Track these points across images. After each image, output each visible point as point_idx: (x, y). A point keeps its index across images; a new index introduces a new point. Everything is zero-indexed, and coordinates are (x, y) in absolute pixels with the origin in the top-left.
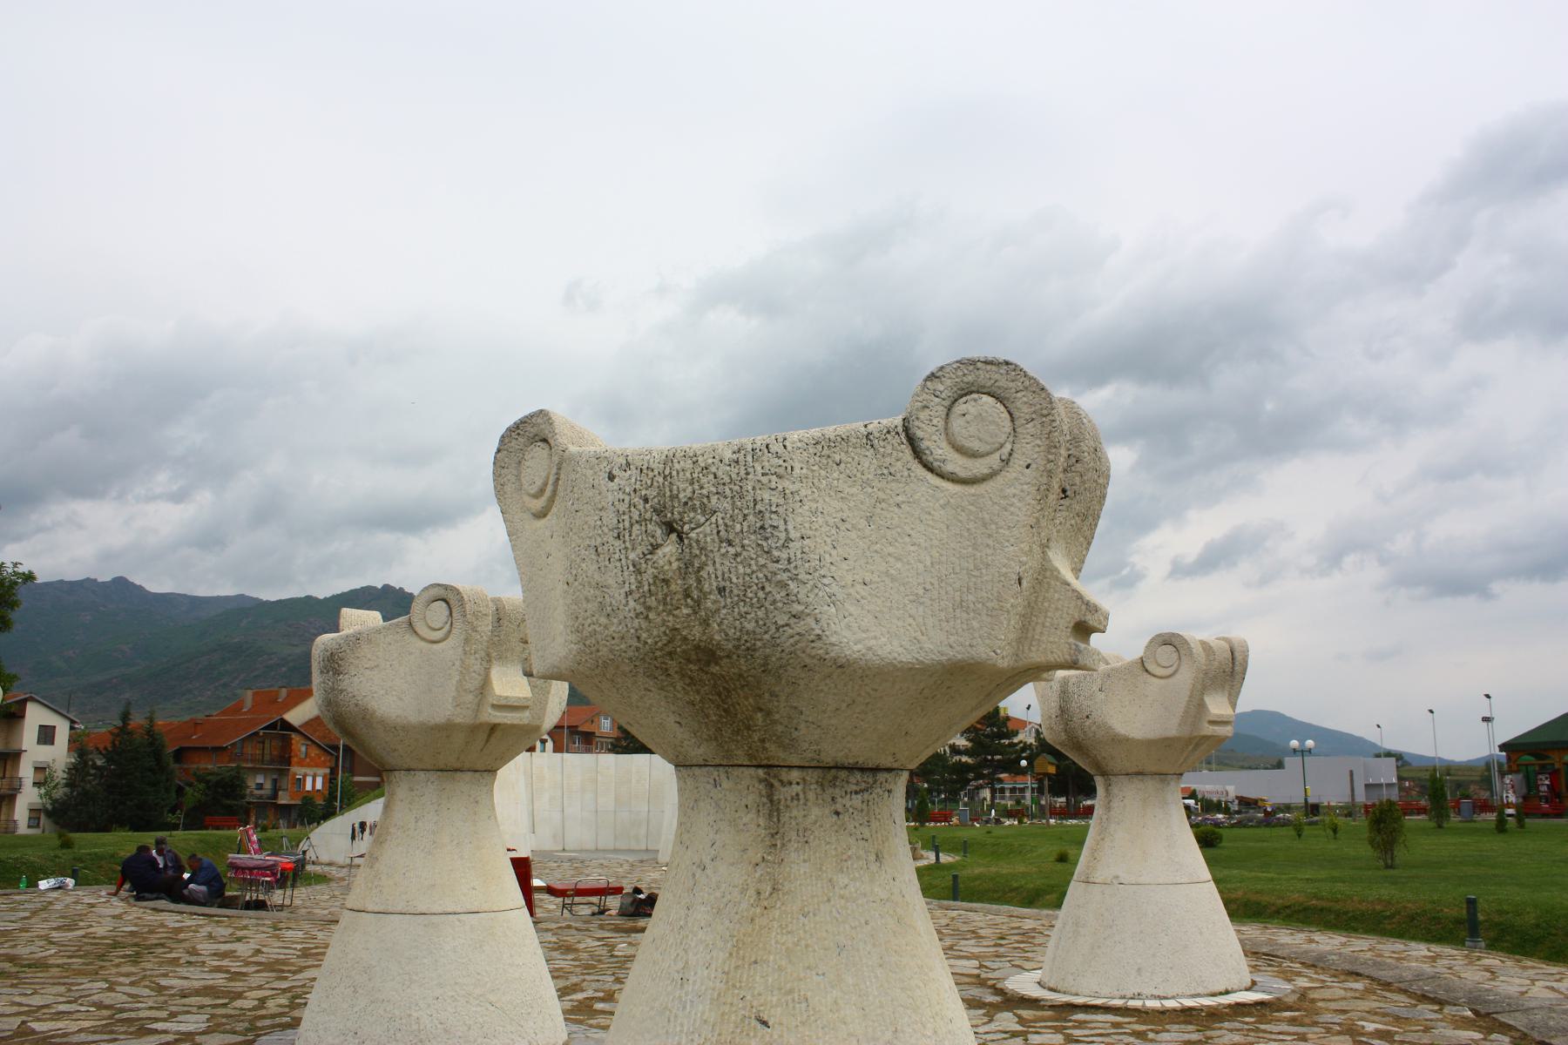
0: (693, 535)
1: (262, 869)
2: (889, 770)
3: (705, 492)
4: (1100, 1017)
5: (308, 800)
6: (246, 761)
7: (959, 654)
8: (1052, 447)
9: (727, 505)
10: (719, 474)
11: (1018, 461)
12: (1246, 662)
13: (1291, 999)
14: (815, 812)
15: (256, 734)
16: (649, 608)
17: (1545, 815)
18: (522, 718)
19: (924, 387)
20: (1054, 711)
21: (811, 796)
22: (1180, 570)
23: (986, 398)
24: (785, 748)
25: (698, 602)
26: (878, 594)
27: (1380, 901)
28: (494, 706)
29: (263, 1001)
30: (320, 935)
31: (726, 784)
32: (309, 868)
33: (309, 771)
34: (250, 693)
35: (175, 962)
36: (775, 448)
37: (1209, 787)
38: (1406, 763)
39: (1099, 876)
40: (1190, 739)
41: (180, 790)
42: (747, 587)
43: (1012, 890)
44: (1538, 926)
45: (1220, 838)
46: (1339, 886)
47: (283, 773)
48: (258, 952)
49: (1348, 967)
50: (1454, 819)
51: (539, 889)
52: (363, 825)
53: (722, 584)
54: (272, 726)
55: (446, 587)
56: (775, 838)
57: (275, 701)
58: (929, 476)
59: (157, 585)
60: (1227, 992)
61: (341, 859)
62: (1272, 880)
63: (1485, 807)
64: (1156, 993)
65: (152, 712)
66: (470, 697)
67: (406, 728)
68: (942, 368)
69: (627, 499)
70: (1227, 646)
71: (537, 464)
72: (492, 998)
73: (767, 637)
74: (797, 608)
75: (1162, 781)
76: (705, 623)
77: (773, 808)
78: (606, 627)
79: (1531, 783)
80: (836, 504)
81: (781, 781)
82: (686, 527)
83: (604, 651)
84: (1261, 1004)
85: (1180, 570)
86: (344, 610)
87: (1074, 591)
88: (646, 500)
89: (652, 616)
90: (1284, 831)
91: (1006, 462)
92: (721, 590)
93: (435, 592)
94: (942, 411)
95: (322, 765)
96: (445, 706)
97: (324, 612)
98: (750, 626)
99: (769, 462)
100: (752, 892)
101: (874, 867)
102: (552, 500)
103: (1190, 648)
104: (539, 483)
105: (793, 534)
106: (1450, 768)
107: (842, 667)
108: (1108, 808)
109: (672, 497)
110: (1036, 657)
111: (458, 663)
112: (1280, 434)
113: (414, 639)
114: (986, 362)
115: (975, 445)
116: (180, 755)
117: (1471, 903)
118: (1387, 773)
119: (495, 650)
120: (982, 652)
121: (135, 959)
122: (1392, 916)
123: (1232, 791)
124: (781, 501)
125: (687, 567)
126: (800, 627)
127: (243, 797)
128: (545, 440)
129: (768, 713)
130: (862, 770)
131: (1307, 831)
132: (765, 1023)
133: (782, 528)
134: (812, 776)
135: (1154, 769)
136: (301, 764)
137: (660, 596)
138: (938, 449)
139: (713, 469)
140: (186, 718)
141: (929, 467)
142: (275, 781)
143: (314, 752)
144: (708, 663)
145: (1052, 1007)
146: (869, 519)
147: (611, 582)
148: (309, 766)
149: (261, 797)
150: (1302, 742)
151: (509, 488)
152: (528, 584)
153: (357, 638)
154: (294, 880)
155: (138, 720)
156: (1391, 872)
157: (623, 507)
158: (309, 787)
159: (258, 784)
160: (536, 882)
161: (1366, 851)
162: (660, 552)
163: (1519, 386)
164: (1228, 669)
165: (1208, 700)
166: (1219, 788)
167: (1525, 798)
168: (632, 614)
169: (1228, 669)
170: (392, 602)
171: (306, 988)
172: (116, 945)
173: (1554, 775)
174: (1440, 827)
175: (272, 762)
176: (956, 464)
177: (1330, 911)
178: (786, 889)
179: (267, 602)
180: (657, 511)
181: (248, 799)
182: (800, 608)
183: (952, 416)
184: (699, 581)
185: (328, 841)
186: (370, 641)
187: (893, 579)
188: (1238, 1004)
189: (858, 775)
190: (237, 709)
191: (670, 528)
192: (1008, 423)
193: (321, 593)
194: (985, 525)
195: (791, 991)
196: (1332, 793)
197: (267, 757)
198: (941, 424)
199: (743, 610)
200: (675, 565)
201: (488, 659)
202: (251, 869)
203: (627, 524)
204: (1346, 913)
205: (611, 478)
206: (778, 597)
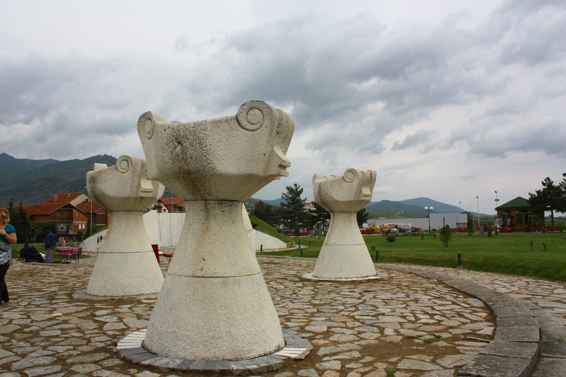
1: (68, 251)
4: (327, 283)
5: (80, 233)
6: (57, 219)
8: (272, 122)
11: (264, 126)
14: (217, 211)
15: (60, 209)
17: (509, 232)
18: (151, 195)
20: (317, 193)
21: (216, 207)
22: (397, 147)
26: (228, 159)
27: (438, 256)
29: (74, 284)
30: (90, 269)
31: (196, 205)
32: (83, 254)
33: (80, 222)
34: (57, 195)
35: (44, 276)
36: (204, 123)
37: (402, 224)
40: (357, 201)
41: (33, 230)
42: (197, 157)
44: (482, 262)
47: (71, 223)
48: (70, 273)
49: (410, 271)
51: (161, 255)
52: (101, 237)
54: (66, 207)
55: (127, 156)
56: (207, 217)
57: (66, 198)
58: (242, 129)
59: (18, 156)
60: (367, 277)
61: (94, 250)
65: (21, 202)
67: (116, 199)
72: (144, 276)
74: (209, 161)
76: (188, 165)
77: (207, 210)
79: (504, 221)
80: (219, 137)
83: (165, 173)
85: (397, 147)
86: (95, 164)
90: (418, 237)
91: (261, 126)
92: (191, 157)
94: (245, 113)
95: (85, 220)
96: (127, 191)
97: (90, 163)
98: (198, 166)
100: (202, 230)
101: (232, 224)
102: (152, 135)
104: (149, 130)
105: (208, 144)
108: (334, 223)
112: (436, 97)
113: (117, 172)
115: (254, 122)
116: (32, 217)
117: (459, 255)
120: (255, 172)
121: (32, 276)
122: (440, 261)
123: (410, 225)
125: (183, 152)
126: (210, 166)
127: (56, 232)
129: (204, 187)
130: (229, 201)
134: (216, 202)
136: (77, 220)
138: (244, 123)
140: (33, 204)
142: (67, 226)
143: (81, 215)
145: (314, 281)
146: (227, 140)
148: (80, 220)
149: (63, 232)
150: (429, 207)
151: (141, 131)
152: (147, 156)
153: (100, 172)
154: (78, 257)
155: (16, 205)
157: (168, 138)
158: (80, 228)
159: (61, 227)
160: (160, 253)
163: (523, 81)
164: (370, 180)
165: (363, 189)
166: (405, 224)
167: (502, 226)
169: (370, 180)
170: (110, 161)
171: (87, 281)
172: (24, 273)
173: (512, 218)
174: (470, 235)
175: (66, 219)
176: (249, 126)
179: (61, 162)
180: (176, 139)
181: (58, 233)
185: (90, 244)
186: (104, 173)
187: (233, 154)
189: (228, 202)
190: (53, 200)
192: (262, 117)
193: (82, 157)
197: (64, 218)
198: (245, 117)
201: (140, 177)
202: (64, 251)
205: (165, 130)
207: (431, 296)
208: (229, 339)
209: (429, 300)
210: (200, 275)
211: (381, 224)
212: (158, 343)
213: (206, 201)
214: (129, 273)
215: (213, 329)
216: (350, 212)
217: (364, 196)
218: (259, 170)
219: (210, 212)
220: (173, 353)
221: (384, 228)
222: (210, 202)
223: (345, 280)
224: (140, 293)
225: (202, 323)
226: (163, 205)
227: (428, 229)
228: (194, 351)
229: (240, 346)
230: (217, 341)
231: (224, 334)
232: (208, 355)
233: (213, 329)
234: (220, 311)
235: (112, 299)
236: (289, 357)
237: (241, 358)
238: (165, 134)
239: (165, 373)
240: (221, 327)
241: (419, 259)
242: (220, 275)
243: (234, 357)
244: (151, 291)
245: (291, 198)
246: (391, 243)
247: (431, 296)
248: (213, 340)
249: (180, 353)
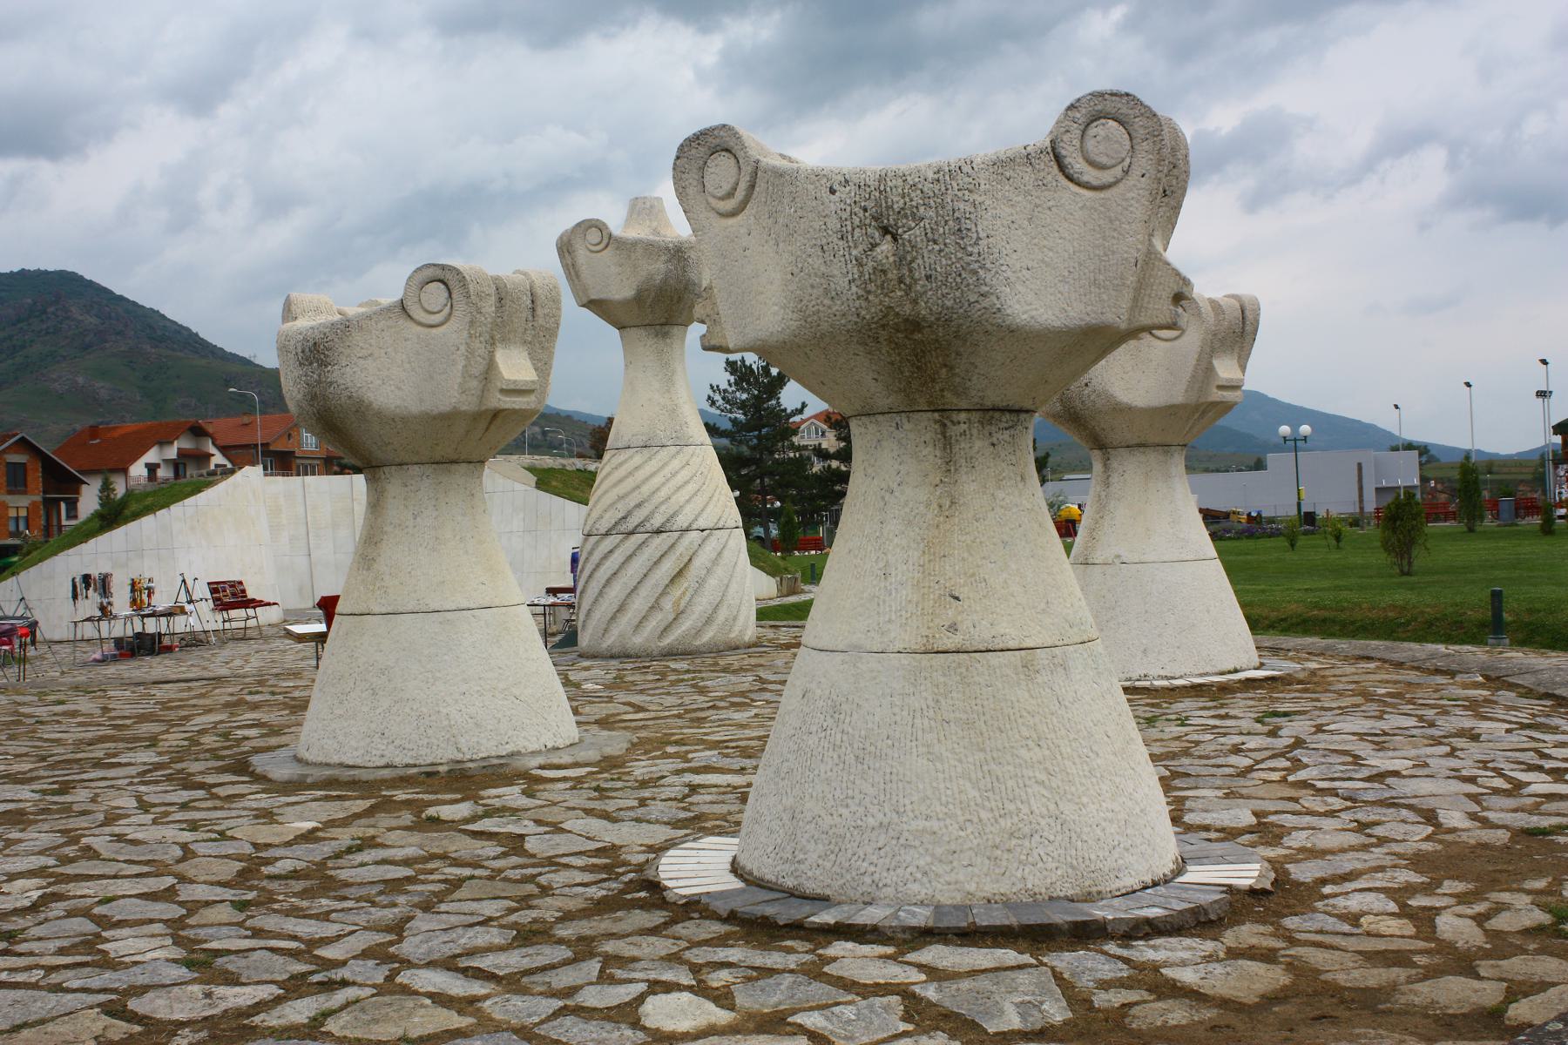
0: (906, 236)
2: (1027, 411)
7: (1092, 319)
9: (932, 213)
11: (1136, 172)
12: (1257, 322)
13: (1301, 676)
14: (978, 444)
16: (869, 292)
19: (1066, 115)
21: (975, 432)
23: (1111, 123)
24: (957, 395)
25: (910, 287)
27: (1393, 607)
28: (502, 391)
31: (907, 426)
36: (966, 169)
38: (1432, 459)
39: (1098, 557)
40: (1197, 407)
42: (948, 274)
46: (1345, 594)
50: (1488, 523)
55: (443, 267)
56: (949, 464)
58: (1071, 185)
60: (1236, 671)
62: (1263, 591)
63: (1530, 508)
64: (1163, 673)
66: (474, 383)
70: (1238, 305)
71: (721, 172)
72: (516, 691)
75: (1166, 452)
76: (915, 302)
77: (946, 442)
80: (1008, 210)
84: (1267, 679)
88: (865, 210)
91: (1126, 172)
92: (928, 277)
93: (429, 273)
96: (450, 391)
98: (949, 303)
99: (963, 180)
100: (935, 506)
101: (1021, 485)
103: (1198, 308)
105: (982, 235)
106: (1493, 464)
107: (1015, 334)
109: (888, 208)
110: (1145, 320)
111: (463, 348)
113: (409, 324)
114: (1112, 94)
115: (1104, 160)
118: (1406, 474)
119: (499, 333)
120: (1110, 317)
122: (1408, 623)
125: (901, 260)
126: (985, 303)
128: (727, 150)
129: (952, 368)
131: (1302, 541)
132: (957, 599)
134: (975, 416)
135: (1157, 440)
138: (1077, 165)
141: (1070, 178)
144: (912, 332)
147: (836, 272)
150: (1295, 428)
151: (691, 191)
156: (1405, 579)
161: (1380, 558)
162: (878, 250)
165: (1216, 363)
174: (1471, 530)
176: (1090, 175)
177: (1334, 621)
183: (1087, 138)
187: (1047, 265)
188: (1248, 680)
191: (885, 231)
192: (1128, 143)
195: (973, 575)
196: (1333, 496)
198: (1076, 142)
200: (891, 259)
201: (492, 342)
204: (1353, 623)
205: (833, 192)
207: (1510, 722)
208: (1059, 838)
209: (1508, 731)
210: (950, 645)
212: (828, 865)
213: (944, 413)
214: (465, 681)
215: (1012, 807)
216: (1165, 447)
217: (1221, 387)
218: (1116, 313)
219: (956, 449)
220: (889, 891)
222: (955, 417)
223: (1165, 683)
224: (510, 748)
225: (973, 793)
226: (212, 450)
227: (1294, 512)
228: (961, 877)
229: (1093, 857)
230: (1027, 843)
231: (1043, 823)
232: (1004, 887)
233: (1012, 807)
234: (1023, 752)
235: (429, 774)
236: (1230, 886)
237: (1099, 893)
238: (832, 204)
239: (905, 941)
240: (1032, 801)
241: (1324, 621)
242: (1012, 644)
243: (1078, 890)
244: (542, 740)
245: (743, 405)
247: (1510, 722)
248: (1014, 842)
249: (915, 887)
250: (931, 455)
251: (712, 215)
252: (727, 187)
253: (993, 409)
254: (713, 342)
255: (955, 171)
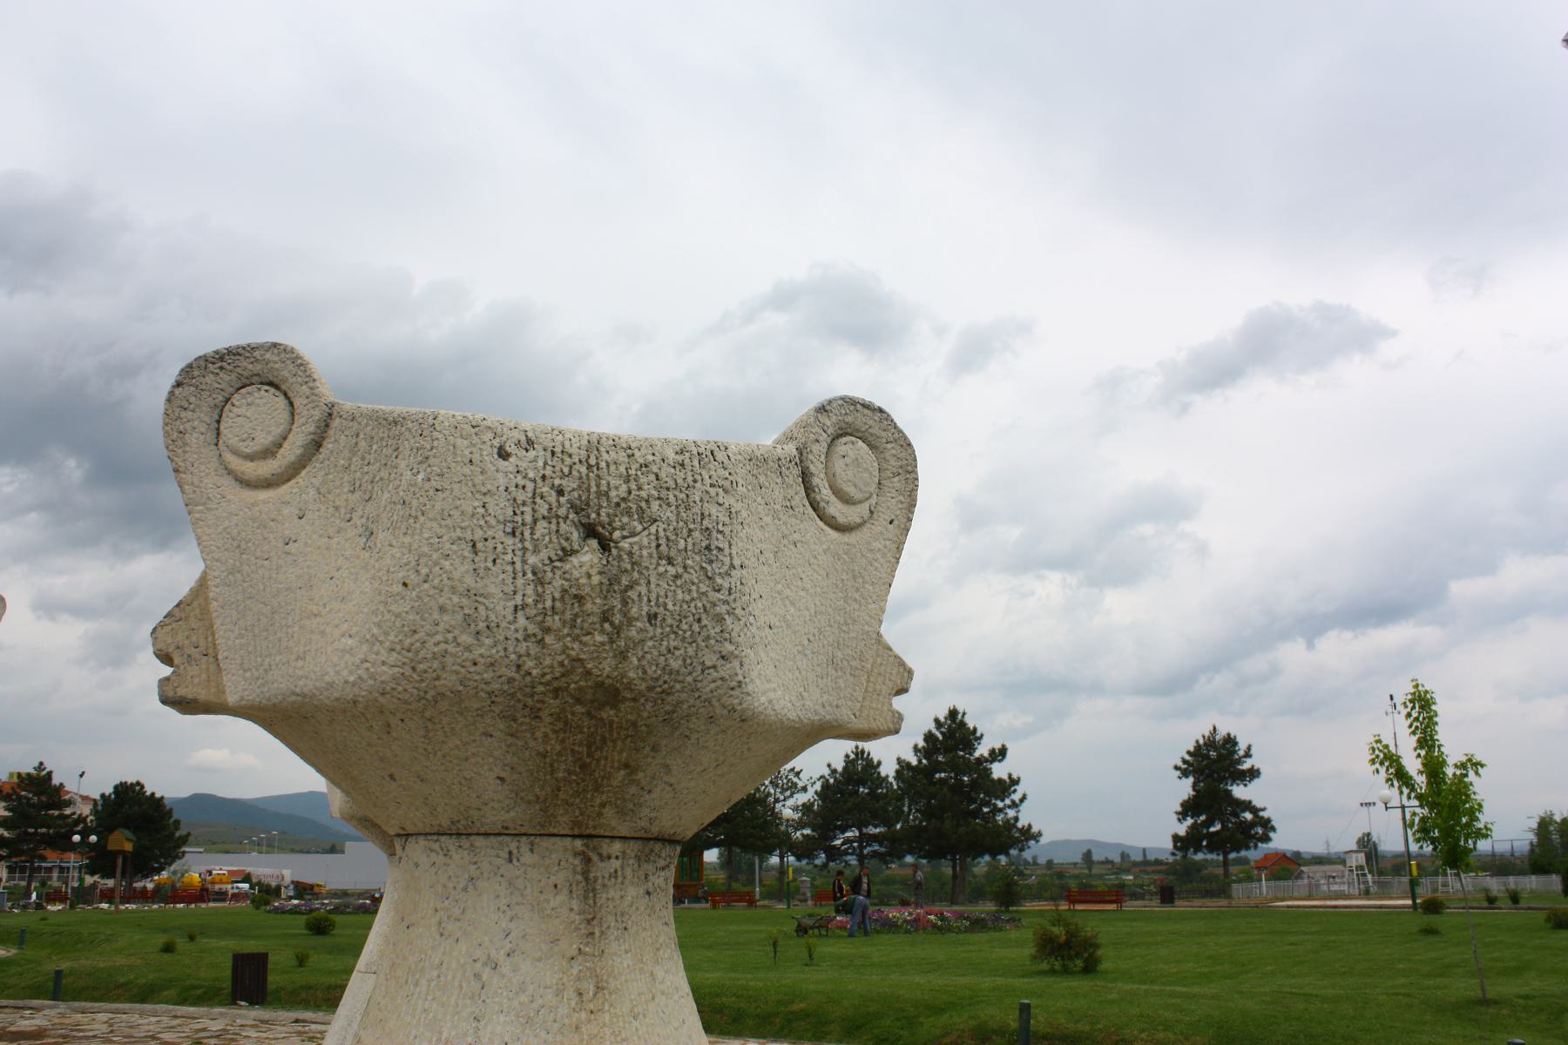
0: (625, 545)
3: (643, 494)
9: (669, 514)
10: (663, 475)
14: (632, 892)
16: (547, 630)
21: (628, 872)
24: (621, 812)
25: (618, 630)
31: (527, 858)
36: (720, 456)
43: (121, 986)
45: (332, 925)
53: (654, 609)
56: (591, 924)
68: (830, 402)
69: (530, 486)
71: (256, 417)
73: (689, 679)
76: (622, 655)
77: (589, 887)
78: (468, 649)
81: (600, 855)
82: (617, 534)
87: (896, 657)
88: (560, 492)
89: (549, 639)
92: (652, 617)
98: (675, 664)
100: (570, 993)
105: (737, 562)
109: (599, 494)
115: (851, 490)
123: (288, 875)
124: (727, 520)
133: (727, 551)
134: (633, 848)
137: (568, 616)
139: (655, 469)
144: (601, 706)
147: (492, 589)
151: (193, 439)
162: (575, 560)
166: (276, 872)
168: (520, 636)
176: (835, 508)
178: (612, 986)
182: (731, 648)
184: (625, 602)
191: (590, 531)
194: (854, 577)
199: (673, 644)
200: (596, 579)
203: (528, 519)
205: (503, 454)
206: (712, 632)
211: (203, 869)
213: (589, 837)
221: (213, 883)
238: (501, 475)
246: (320, 940)
250: (564, 906)
251: (228, 482)
252: (263, 440)
253: (657, 839)
254: (182, 692)
255: (709, 455)
